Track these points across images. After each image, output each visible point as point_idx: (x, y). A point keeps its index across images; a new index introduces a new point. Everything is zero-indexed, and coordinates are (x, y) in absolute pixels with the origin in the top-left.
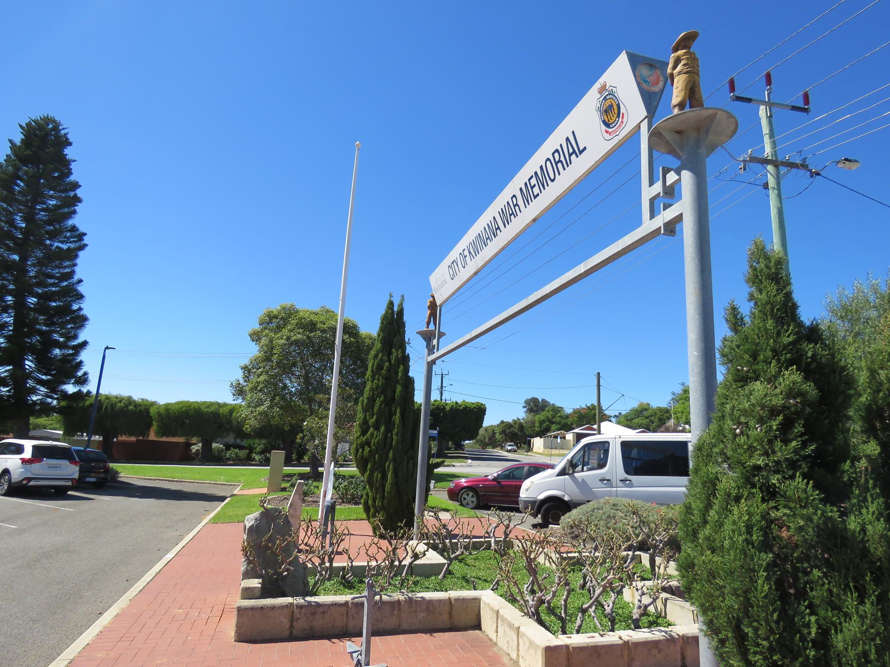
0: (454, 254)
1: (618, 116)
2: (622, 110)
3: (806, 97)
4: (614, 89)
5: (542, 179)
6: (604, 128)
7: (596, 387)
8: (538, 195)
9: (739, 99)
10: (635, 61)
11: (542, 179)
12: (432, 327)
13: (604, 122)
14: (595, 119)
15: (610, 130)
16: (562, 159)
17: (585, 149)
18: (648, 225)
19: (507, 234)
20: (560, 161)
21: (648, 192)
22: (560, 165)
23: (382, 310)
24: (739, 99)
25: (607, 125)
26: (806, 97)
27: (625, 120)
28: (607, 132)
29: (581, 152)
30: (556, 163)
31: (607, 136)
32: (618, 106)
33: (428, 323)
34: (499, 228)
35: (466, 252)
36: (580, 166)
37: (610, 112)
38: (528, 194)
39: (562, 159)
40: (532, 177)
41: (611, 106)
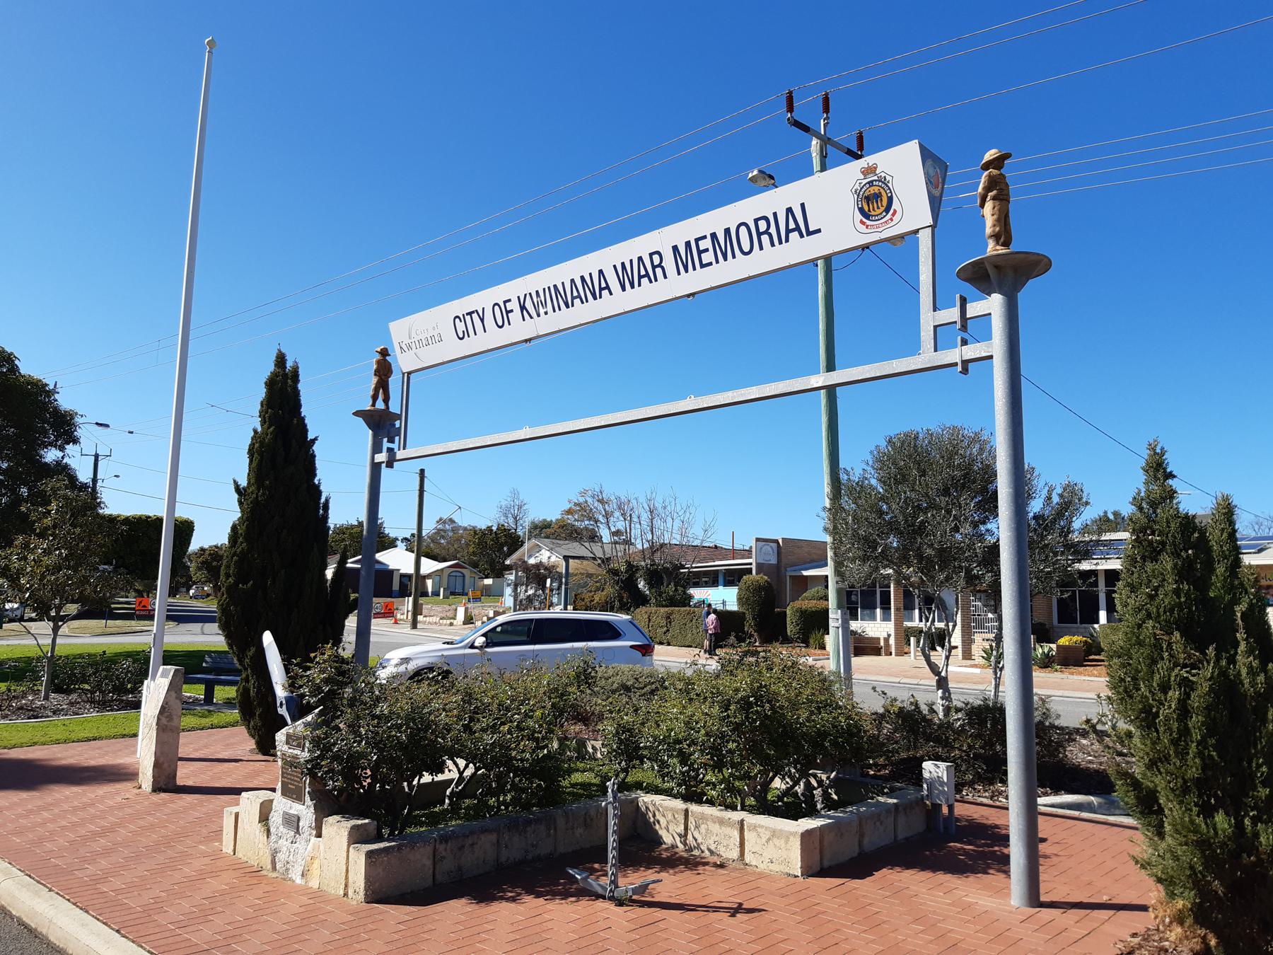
0: (483, 299)
1: (887, 210)
2: (895, 205)
3: (860, 139)
4: (888, 178)
5: (725, 244)
6: (859, 216)
7: (417, 493)
8: (710, 264)
9: (797, 124)
10: (926, 154)
11: (725, 244)
12: (380, 405)
13: (861, 210)
14: (849, 205)
15: (868, 222)
16: (773, 230)
17: (819, 231)
18: (927, 356)
19: (619, 301)
20: (766, 232)
21: (928, 319)
22: (765, 238)
23: (269, 367)
24: (797, 124)
25: (866, 215)
26: (860, 139)
27: (896, 218)
28: (862, 222)
29: (809, 233)
30: (759, 234)
31: (862, 228)
32: (890, 200)
33: (375, 398)
34: (607, 287)
35: (513, 305)
36: (798, 250)
37: (875, 201)
38: (688, 257)
39: (773, 230)
40: (705, 237)
41: (877, 196)
